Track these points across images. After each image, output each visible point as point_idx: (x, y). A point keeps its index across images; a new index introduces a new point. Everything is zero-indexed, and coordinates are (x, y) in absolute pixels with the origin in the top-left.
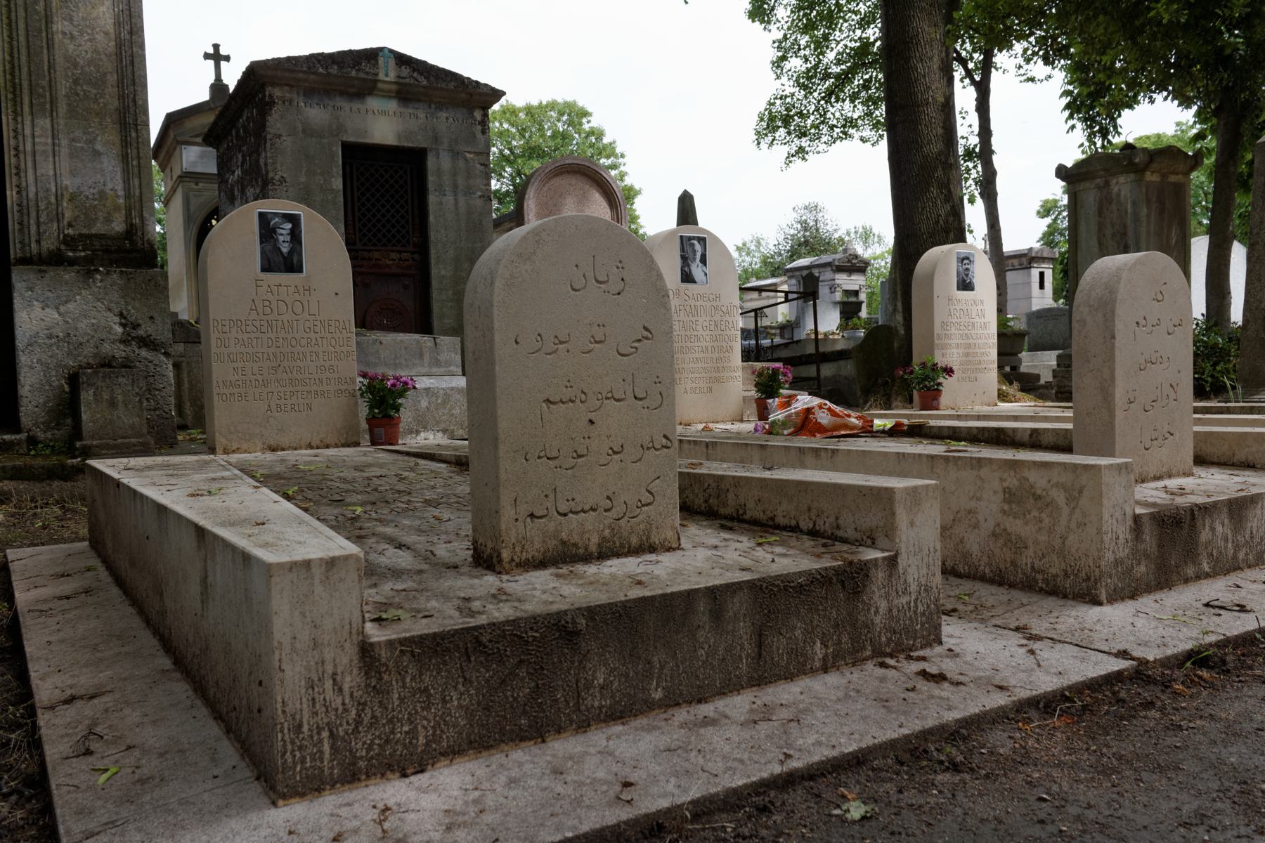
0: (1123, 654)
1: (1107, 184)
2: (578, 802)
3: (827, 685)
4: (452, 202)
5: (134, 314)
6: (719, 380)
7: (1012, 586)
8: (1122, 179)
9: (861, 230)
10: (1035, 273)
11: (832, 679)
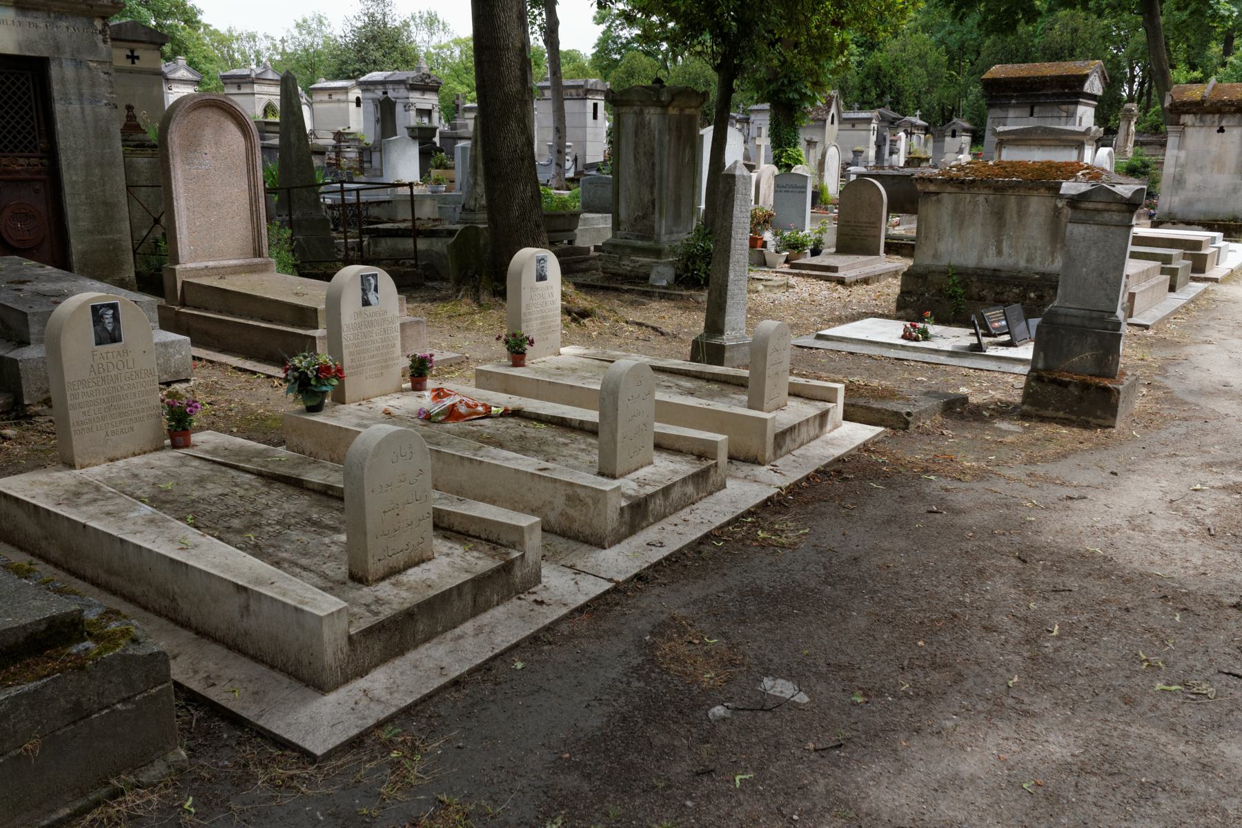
0: (610, 580)
1: (641, 112)
2: (428, 677)
3: (499, 612)
4: (79, 110)
6: (387, 367)
7: (569, 538)
8: (652, 111)
9: (426, 15)
10: (590, 103)
11: (501, 609)
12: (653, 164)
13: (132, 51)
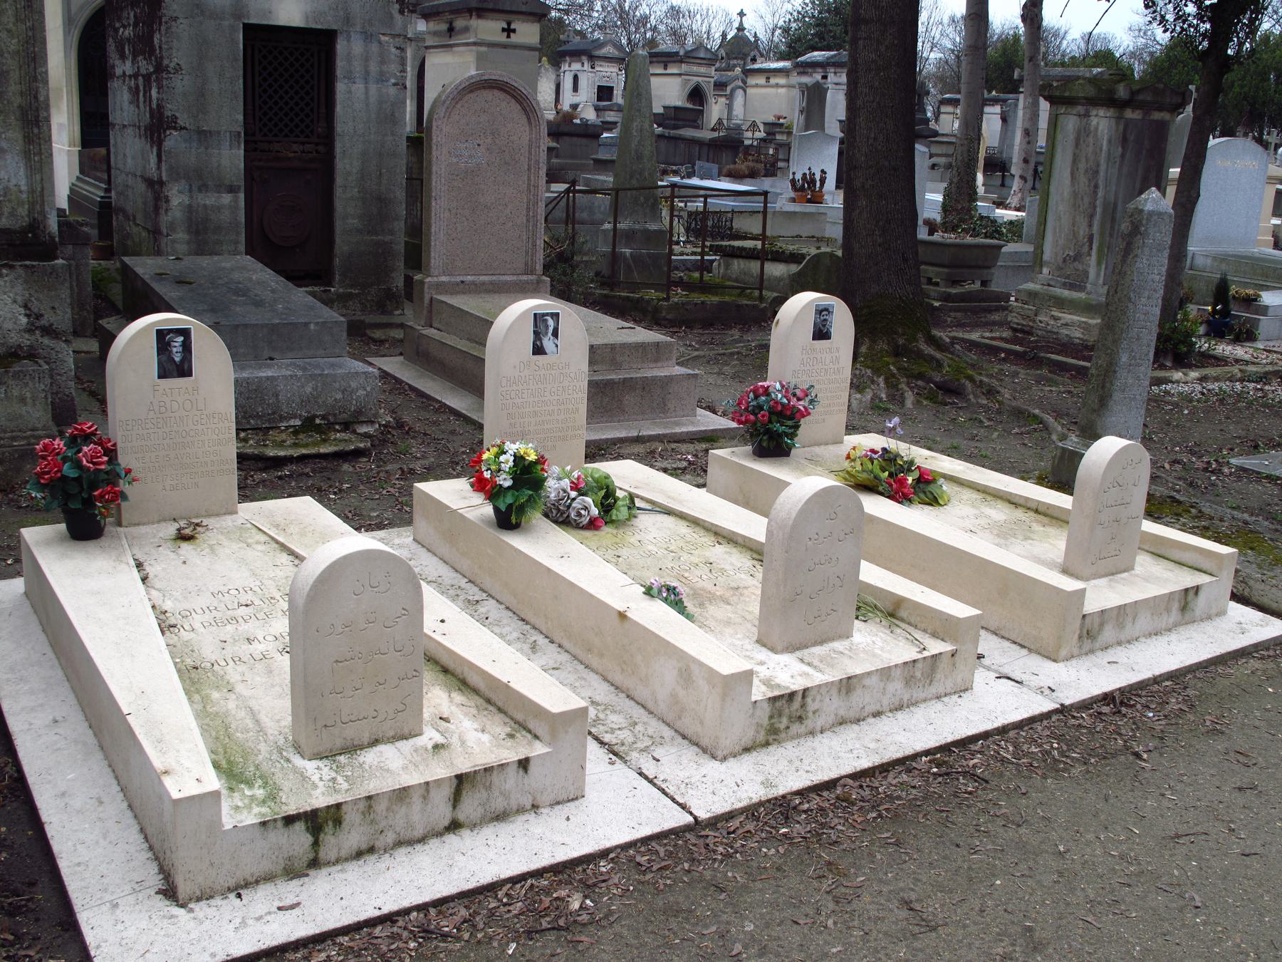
1: (1087, 115)
5: (35, 306)
8: (1102, 112)
12: (1096, 186)
13: (509, 24)
